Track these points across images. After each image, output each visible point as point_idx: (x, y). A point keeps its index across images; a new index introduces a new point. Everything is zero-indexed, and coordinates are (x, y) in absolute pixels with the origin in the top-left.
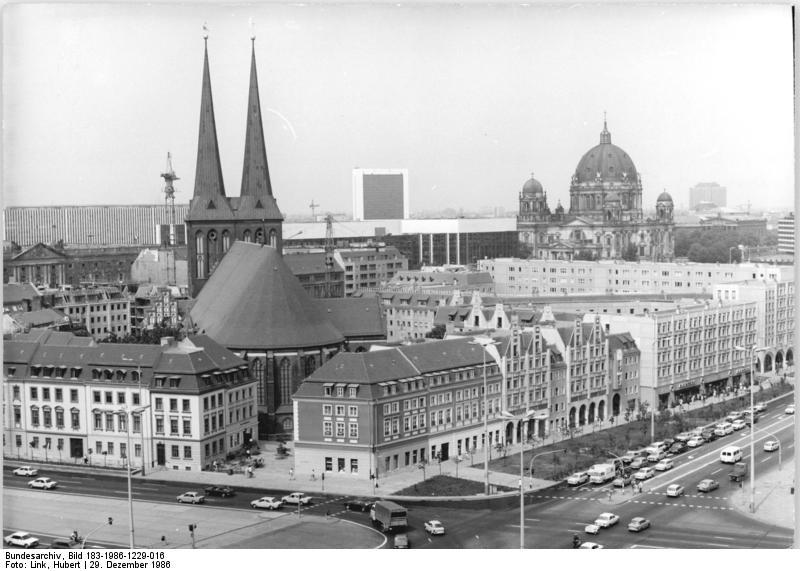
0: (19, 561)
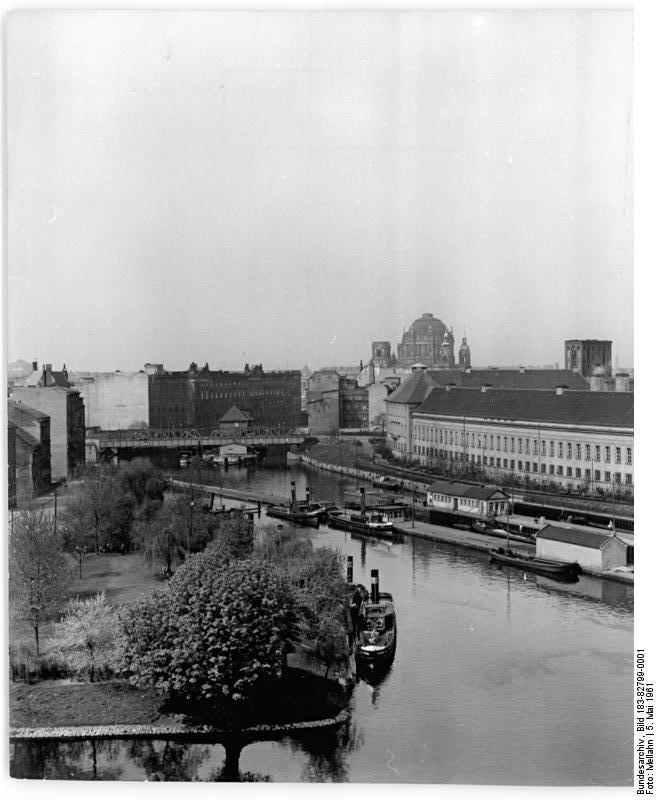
0: (646, 781)
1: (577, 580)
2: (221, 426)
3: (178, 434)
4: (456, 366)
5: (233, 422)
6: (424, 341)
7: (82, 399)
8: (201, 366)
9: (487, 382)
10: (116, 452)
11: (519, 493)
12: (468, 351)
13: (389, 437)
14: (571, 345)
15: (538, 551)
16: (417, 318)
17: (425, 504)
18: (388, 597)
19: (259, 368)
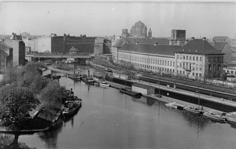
1: (140, 98)
2: (69, 52)
3: (85, 54)
4: (147, 37)
5: (73, 51)
6: (137, 29)
7: (24, 43)
8: (67, 34)
9: (137, 42)
10: (39, 59)
11: (141, 73)
12: (151, 32)
13: (113, 57)
14: (173, 31)
15: (132, 89)
16: (136, 22)
17: (112, 75)
18: (81, 100)
19: (85, 36)
